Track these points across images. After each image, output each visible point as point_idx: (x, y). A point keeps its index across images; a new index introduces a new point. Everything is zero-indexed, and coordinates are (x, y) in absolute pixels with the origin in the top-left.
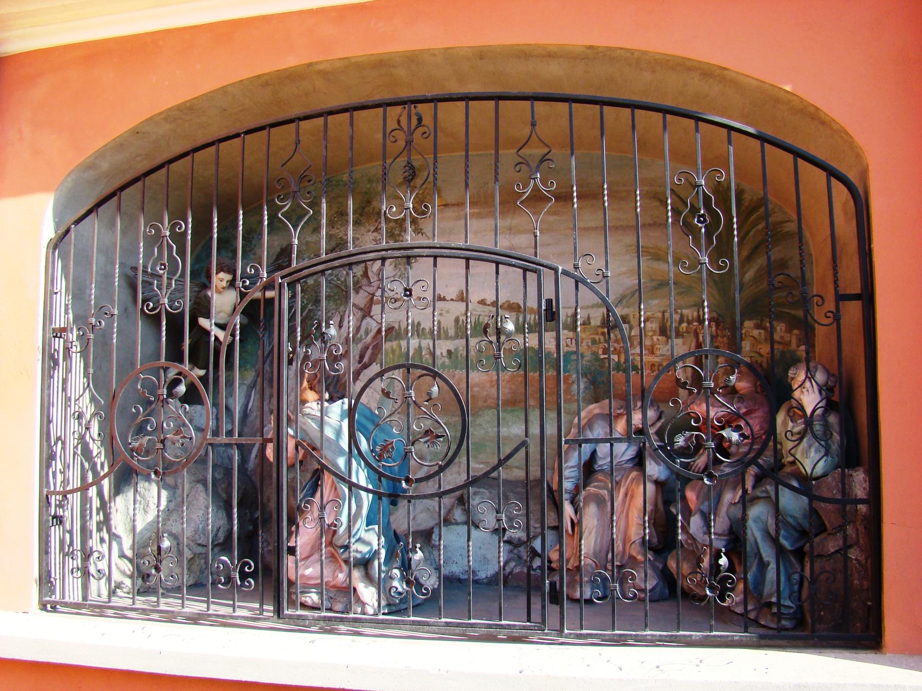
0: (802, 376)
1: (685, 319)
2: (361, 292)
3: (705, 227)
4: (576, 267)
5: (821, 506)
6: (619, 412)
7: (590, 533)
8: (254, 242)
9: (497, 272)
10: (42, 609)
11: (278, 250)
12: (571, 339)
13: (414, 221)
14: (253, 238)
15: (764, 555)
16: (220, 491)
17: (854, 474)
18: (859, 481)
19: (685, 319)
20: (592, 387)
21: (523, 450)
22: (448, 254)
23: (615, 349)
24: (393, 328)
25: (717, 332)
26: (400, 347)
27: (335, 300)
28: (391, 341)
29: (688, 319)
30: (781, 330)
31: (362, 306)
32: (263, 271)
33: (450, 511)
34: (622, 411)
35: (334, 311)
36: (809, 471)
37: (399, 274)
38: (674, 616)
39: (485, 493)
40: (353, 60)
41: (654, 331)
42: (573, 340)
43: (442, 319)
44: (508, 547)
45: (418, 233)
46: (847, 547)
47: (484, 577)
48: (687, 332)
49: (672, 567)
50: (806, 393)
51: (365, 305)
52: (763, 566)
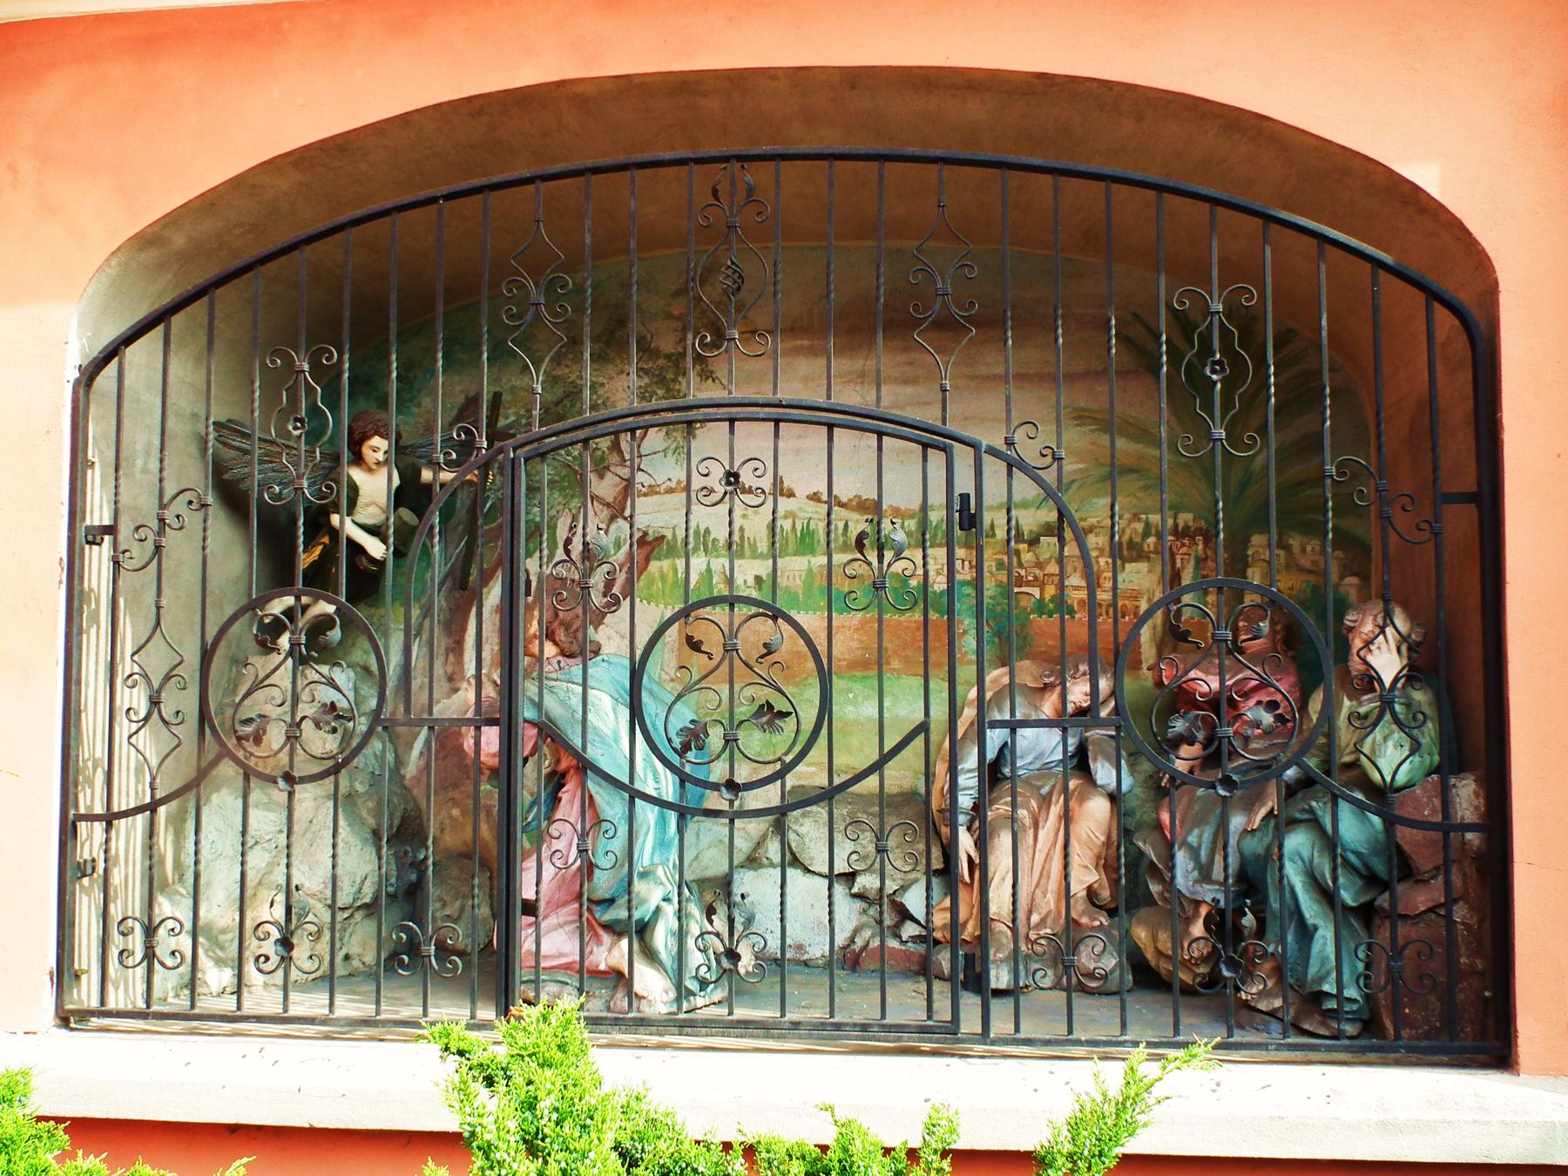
0: (1368, 627)
1: (1153, 530)
2: (609, 475)
3: (1222, 381)
4: (1010, 443)
5: (1404, 835)
6: (1047, 680)
7: (1003, 879)
8: (417, 386)
9: (880, 448)
10: (58, 1026)
11: (461, 399)
12: (963, 561)
13: (699, 359)
14: (415, 378)
15: (1307, 915)
16: (364, 814)
17: (1459, 784)
18: (1466, 796)
19: (1153, 530)
20: (997, 640)
21: (919, 742)
22: (761, 416)
23: (1036, 578)
24: (663, 537)
25: (1205, 553)
26: (675, 570)
27: (563, 489)
28: (659, 559)
29: (1157, 530)
30: (1313, 550)
31: (610, 499)
32: (481, 437)
33: (759, 844)
34: (1052, 679)
35: (561, 507)
36: (1388, 779)
37: (674, 446)
38: (1170, 1012)
39: (818, 812)
40: (636, 81)
41: (1101, 550)
42: (966, 563)
43: (747, 524)
44: (859, 905)
45: (707, 378)
46: (1450, 902)
47: (818, 955)
48: (1155, 552)
49: (1140, 939)
50: (1376, 652)
51: (615, 498)
52: (1306, 933)
